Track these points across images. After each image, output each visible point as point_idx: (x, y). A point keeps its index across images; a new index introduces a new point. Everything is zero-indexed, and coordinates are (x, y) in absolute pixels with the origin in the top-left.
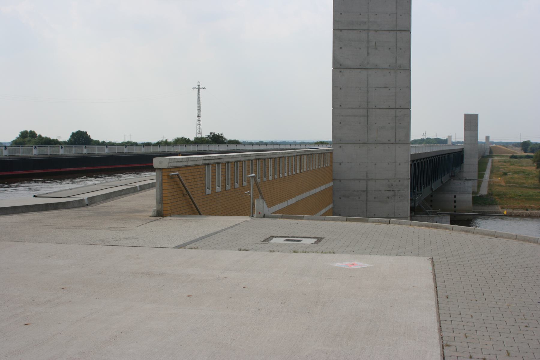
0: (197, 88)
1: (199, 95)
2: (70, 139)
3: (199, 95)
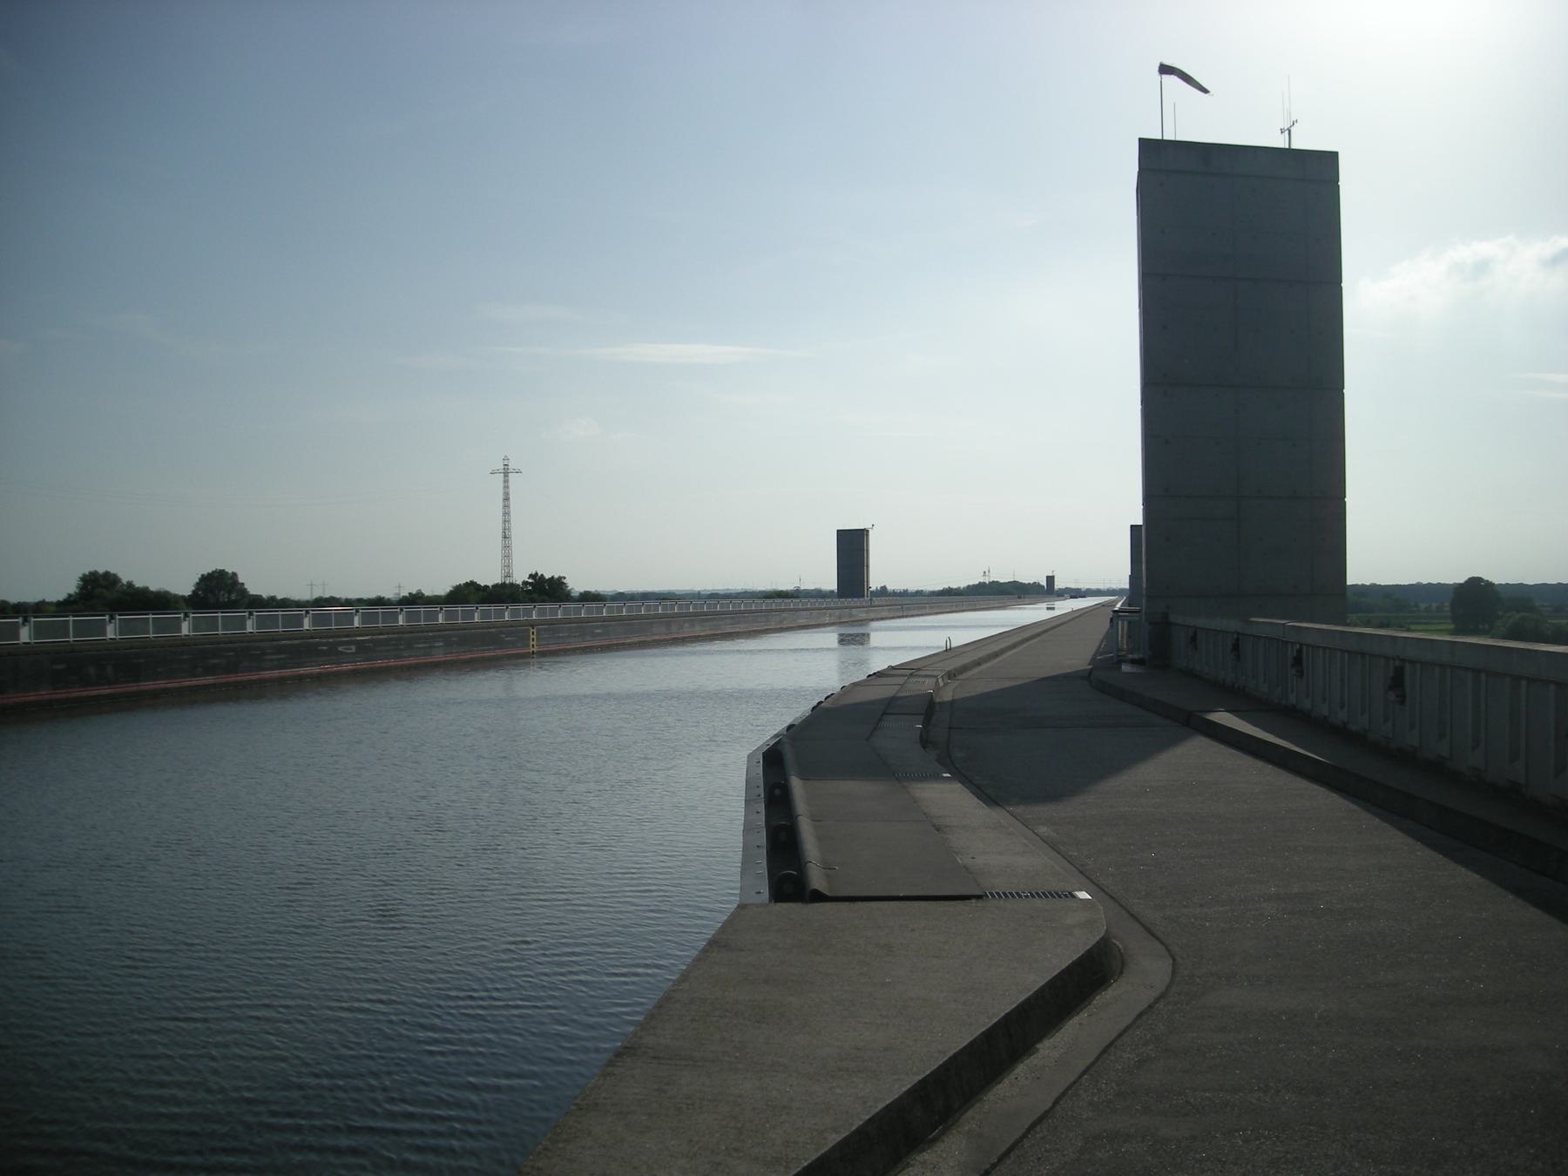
0: (502, 471)
1: (506, 487)
2: (194, 592)
3: (506, 487)
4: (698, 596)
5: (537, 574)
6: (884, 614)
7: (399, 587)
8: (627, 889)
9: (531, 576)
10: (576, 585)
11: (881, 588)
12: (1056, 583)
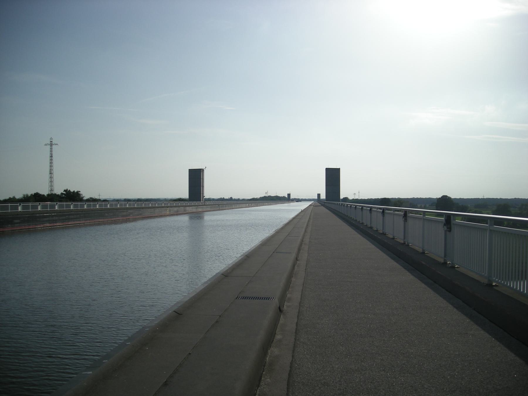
4: (166, 200)
5: (67, 189)
6: (209, 209)
7: (99, 195)
8: (44, 363)
9: (65, 191)
10: (86, 195)
11: (231, 198)
12: (291, 197)
